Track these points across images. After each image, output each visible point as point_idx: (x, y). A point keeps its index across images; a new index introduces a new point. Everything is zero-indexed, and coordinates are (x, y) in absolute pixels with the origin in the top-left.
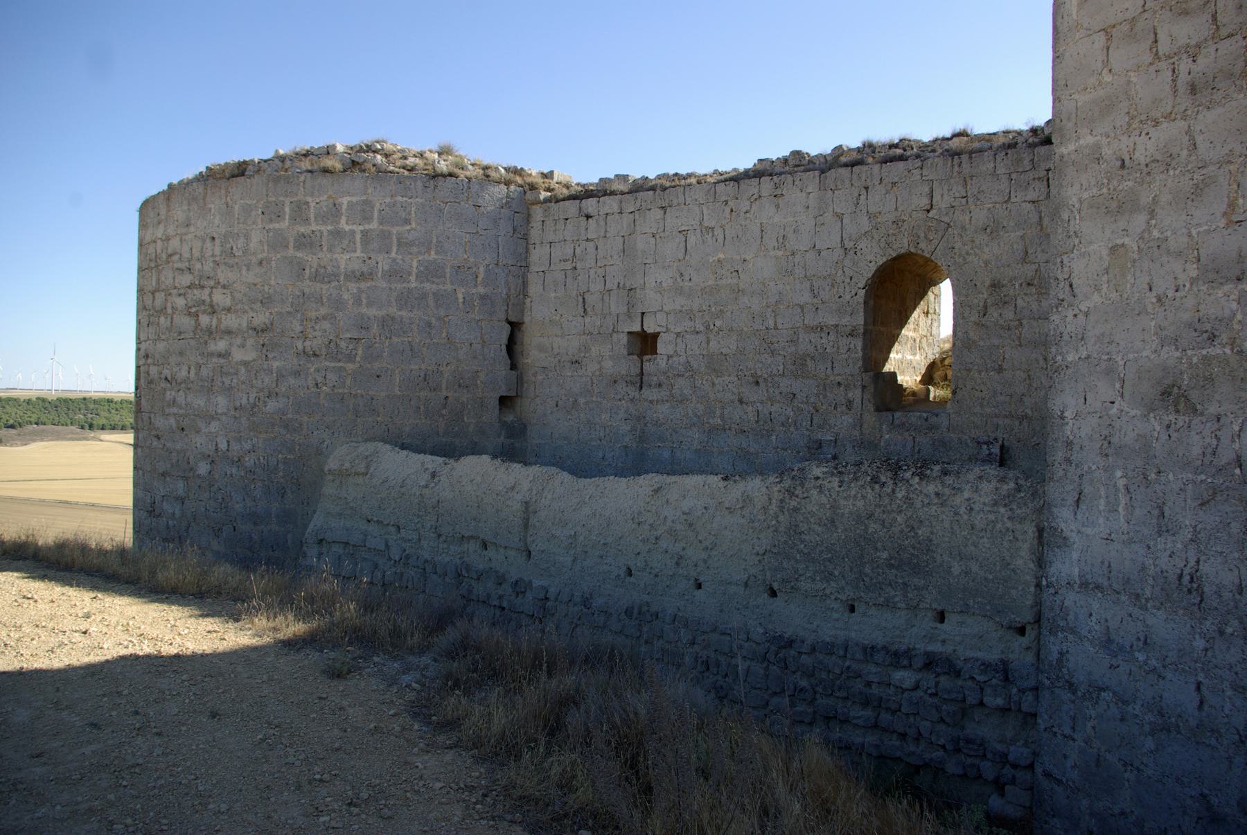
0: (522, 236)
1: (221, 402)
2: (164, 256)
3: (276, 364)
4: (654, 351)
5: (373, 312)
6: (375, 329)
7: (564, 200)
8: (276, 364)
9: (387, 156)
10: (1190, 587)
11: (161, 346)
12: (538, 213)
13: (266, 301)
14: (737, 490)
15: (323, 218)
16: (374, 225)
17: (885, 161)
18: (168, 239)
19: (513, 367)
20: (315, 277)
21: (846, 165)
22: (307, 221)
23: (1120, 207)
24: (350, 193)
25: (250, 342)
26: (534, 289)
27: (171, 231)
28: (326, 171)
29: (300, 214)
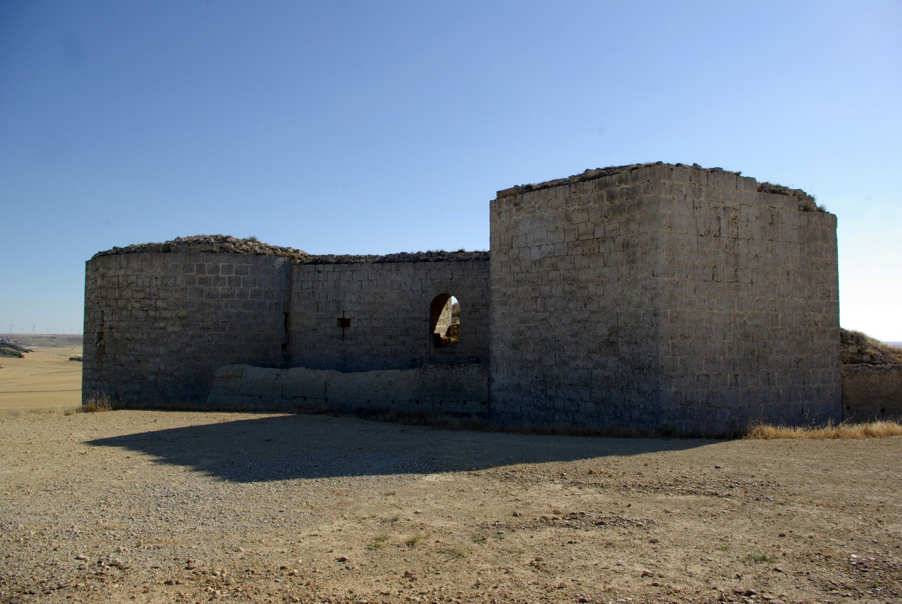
0: (289, 277)
1: (162, 349)
2: (125, 284)
3: (190, 333)
4: (349, 325)
5: (233, 311)
6: (234, 318)
7: (308, 264)
8: (190, 333)
9: (234, 244)
10: (519, 386)
11: (123, 324)
12: (296, 269)
13: (185, 306)
14: (405, 373)
15: (211, 271)
16: (233, 275)
17: (437, 261)
18: (128, 276)
19: (286, 332)
20: (208, 296)
21: (422, 261)
22: (204, 273)
23: (504, 304)
24: (223, 262)
25: (177, 323)
26: (295, 299)
27: (130, 272)
28: (212, 252)
29: (201, 269)
